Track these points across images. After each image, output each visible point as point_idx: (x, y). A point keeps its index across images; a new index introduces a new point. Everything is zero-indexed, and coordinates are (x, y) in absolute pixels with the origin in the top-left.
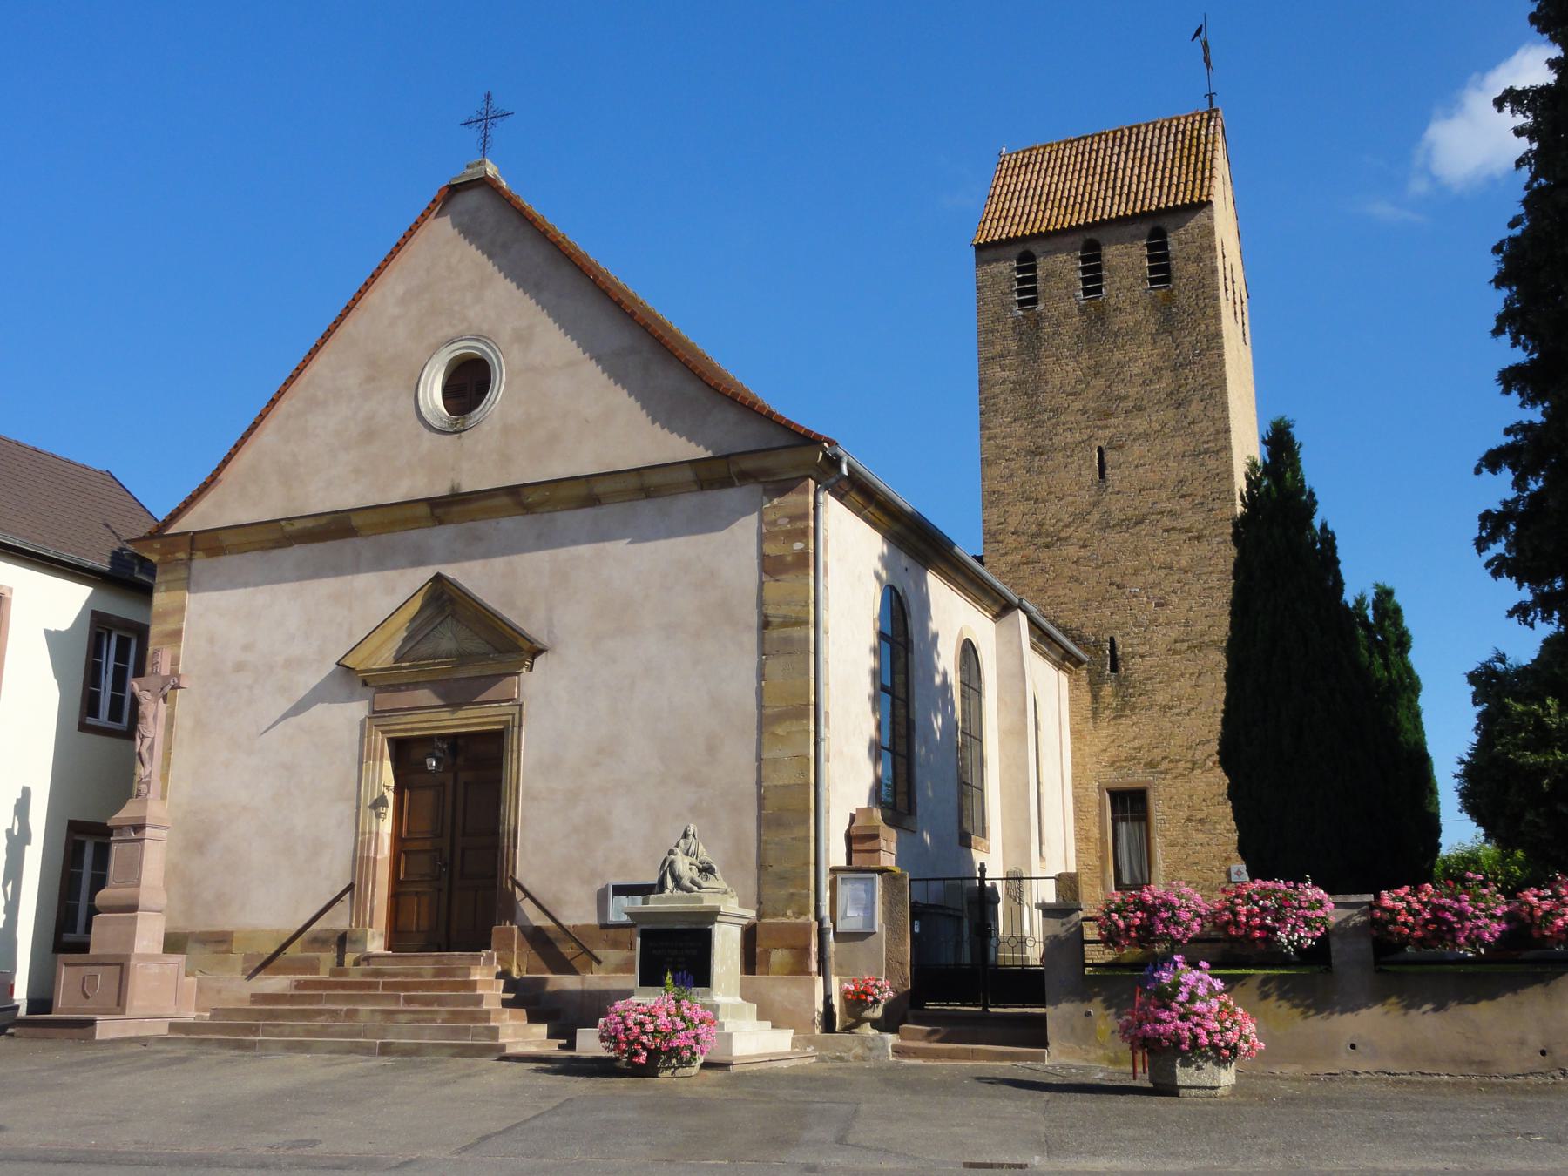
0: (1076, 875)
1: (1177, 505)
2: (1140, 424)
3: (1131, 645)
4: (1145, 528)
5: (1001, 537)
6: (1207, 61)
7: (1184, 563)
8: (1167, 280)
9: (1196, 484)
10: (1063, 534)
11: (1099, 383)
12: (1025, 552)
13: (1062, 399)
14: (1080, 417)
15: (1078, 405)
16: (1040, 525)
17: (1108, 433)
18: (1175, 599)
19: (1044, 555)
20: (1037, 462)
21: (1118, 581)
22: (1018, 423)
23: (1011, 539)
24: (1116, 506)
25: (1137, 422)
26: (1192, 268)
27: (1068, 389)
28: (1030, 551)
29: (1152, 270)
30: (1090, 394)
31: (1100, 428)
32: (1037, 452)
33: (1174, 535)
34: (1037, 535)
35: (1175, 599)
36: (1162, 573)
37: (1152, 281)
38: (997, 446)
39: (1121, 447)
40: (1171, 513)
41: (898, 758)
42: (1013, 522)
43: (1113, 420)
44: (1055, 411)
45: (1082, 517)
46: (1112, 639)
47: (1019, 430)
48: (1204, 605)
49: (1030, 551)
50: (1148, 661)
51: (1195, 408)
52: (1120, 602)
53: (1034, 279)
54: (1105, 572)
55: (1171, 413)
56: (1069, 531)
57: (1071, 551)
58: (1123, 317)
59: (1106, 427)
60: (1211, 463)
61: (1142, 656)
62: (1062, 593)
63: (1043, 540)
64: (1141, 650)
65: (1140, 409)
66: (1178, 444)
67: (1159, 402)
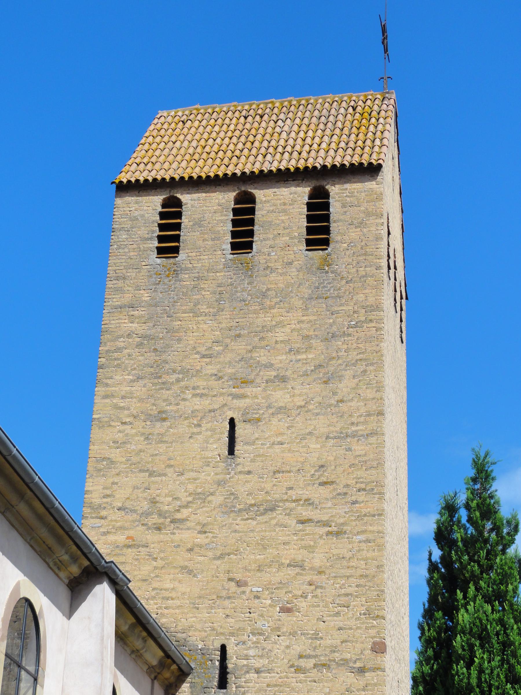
0: (116, 197)
1: (318, 493)
2: (280, 397)
3: (247, 657)
4: (279, 516)
5: (104, 513)
6: (384, 30)
7: (317, 563)
8: (326, 242)
9: (340, 470)
10: (178, 516)
11: (240, 347)
12: (131, 533)
13: (194, 361)
14: (213, 383)
15: (211, 369)
16: (153, 502)
17: (242, 403)
18: (303, 604)
19: (151, 537)
20: (159, 428)
21: (238, 577)
22: (141, 382)
23: (115, 516)
24: (244, 487)
25: (278, 394)
26: (354, 234)
27: (202, 349)
28: (139, 533)
29: (310, 230)
30: (229, 356)
31: (236, 397)
32: (162, 417)
33: (309, 528)
34: (147, 514)
35: (303, 604)
36: (292, 572)
37: (309, 243)
38: (116, 407)
39: (259, 420)
40: (308, 502)
41: (32, 669)
42: (120, 496)
43: (248, 390)
44: (185, 372)
45: (201, 497)
46: (223, 648)
47: (139, 389)
48: (338, 614)
49: (139, 533)
50: (267, 678)
51: (345, 386)
52: (237, 602)
53: (178, 227)
54: (222, 565)
55: (318, 387)
56: (185, 513)
57: (187, 536)
58: (273, 277)
59: (243, 396)
60: (359, 448)
61: (258, 671)
62: (168, 585)
63: (155, 519)
64: (257, 663)
65: (284, 379)
66: (321, 424)
67: (305, 374)
